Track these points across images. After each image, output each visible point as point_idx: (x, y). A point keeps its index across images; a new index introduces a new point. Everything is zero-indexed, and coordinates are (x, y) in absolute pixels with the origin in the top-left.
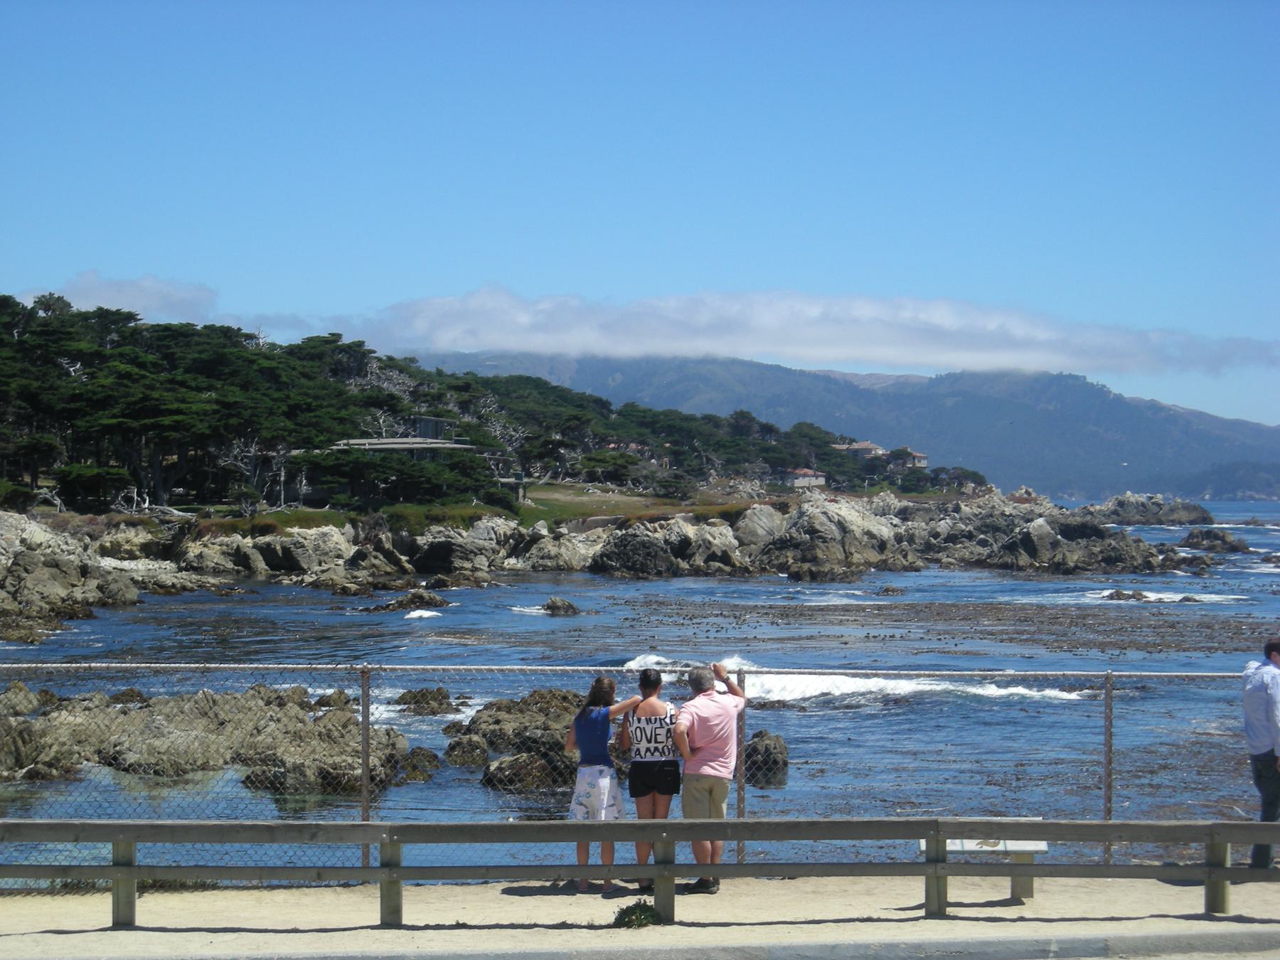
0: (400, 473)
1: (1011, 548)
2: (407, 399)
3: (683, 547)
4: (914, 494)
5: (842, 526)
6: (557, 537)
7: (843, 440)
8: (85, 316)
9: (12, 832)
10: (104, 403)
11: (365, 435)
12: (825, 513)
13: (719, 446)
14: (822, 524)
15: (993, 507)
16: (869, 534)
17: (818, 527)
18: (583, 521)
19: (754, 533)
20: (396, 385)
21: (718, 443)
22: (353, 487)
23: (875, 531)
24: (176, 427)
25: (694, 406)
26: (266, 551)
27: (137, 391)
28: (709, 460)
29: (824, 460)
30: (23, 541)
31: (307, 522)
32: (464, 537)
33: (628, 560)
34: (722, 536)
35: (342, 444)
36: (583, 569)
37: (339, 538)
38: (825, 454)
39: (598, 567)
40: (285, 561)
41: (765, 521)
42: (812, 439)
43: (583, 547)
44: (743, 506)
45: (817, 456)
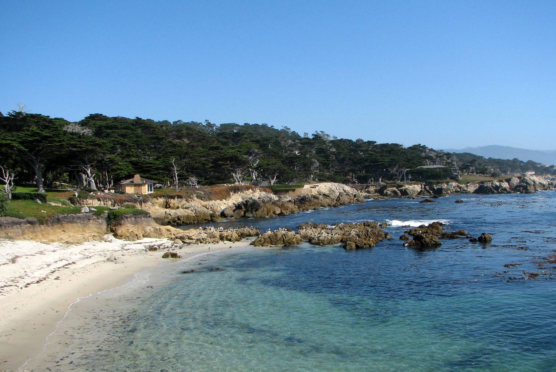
0: (431, 173)
2: (434, 157)
3: (497, 188)
5: (534, 182)
6: (467, 186)
7: (539, 164)
8: (365, 143)
9: (555, 268)
10: (366, 161)
11: (424, 165)
13: (510, 166)
16: (540, 183)
18: (473, 182)
20: (432, 155)
22: (418, 176)
24: (381, 164)
25: (504, 157)
26: (401, 191)
27: (373, 157)
30: (344, 190)
31: (411, 184)
32: (445, 186)
33: (482, 190)
34: (505, 185)
35: (419, 167)
36: (473, 193)
37: (418, 188)
39: (476, 192)
40: (405, 193)
41: (515, 181)
43: (472, 188)
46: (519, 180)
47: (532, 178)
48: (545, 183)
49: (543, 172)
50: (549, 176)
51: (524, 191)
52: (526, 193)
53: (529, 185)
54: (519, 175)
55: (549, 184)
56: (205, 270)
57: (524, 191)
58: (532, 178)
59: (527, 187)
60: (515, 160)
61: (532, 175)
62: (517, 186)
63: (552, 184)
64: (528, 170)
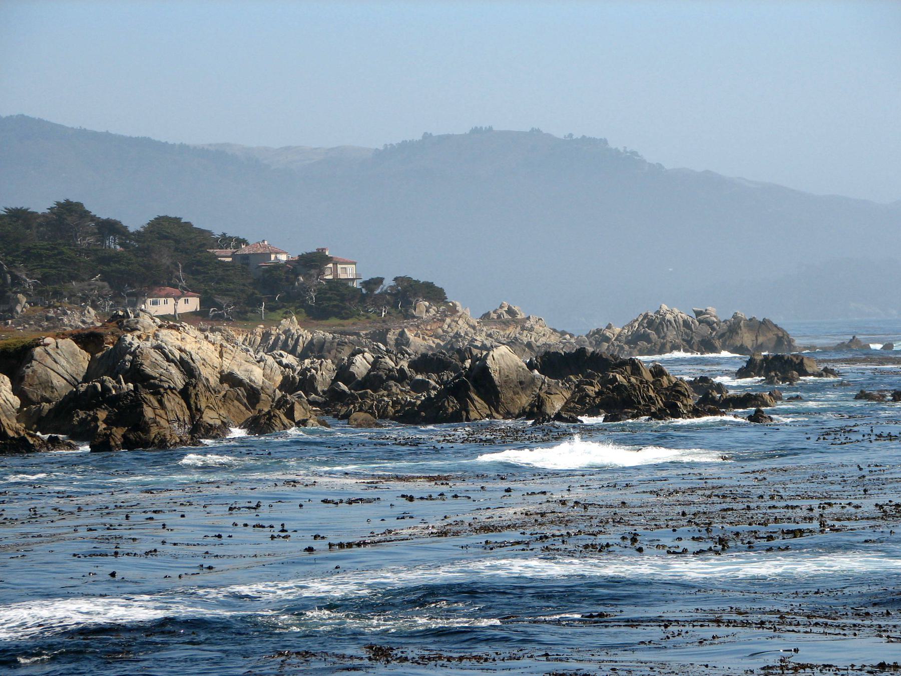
1: (458, 390)
4: (334, 321)
5: (186, 367)
7: (225, 241)
12: (159, 348)
13: (30, 256)
14: (155, 365)
15: (457, 335)
16: (229, 378)
17: (148, 371)
19: (48, 385)
21: (27, 251)
23: (241, 374)
28: (15, 278)
29: (198, 272)
38: (199, 263)
41: (62, 363)
42: (177, 241)
44: (29, 339)
45: (187, 268)
46: (84, 358)
47: (170, 339)
48: (257, 375)
49: (254, 303)
50: (292, 324)
51: (118, 433)
52: (129, 445)
53: (156, 391)
54: (92, 318)
55: (288, 385)
56: (680, 364)
57: (118, 433)
58: (170, 339)
59: (137, 404)
60: (69, 214)
61: (171, 322)
62: (76, 400)
63: (307, 383)
64: (153, 282)
